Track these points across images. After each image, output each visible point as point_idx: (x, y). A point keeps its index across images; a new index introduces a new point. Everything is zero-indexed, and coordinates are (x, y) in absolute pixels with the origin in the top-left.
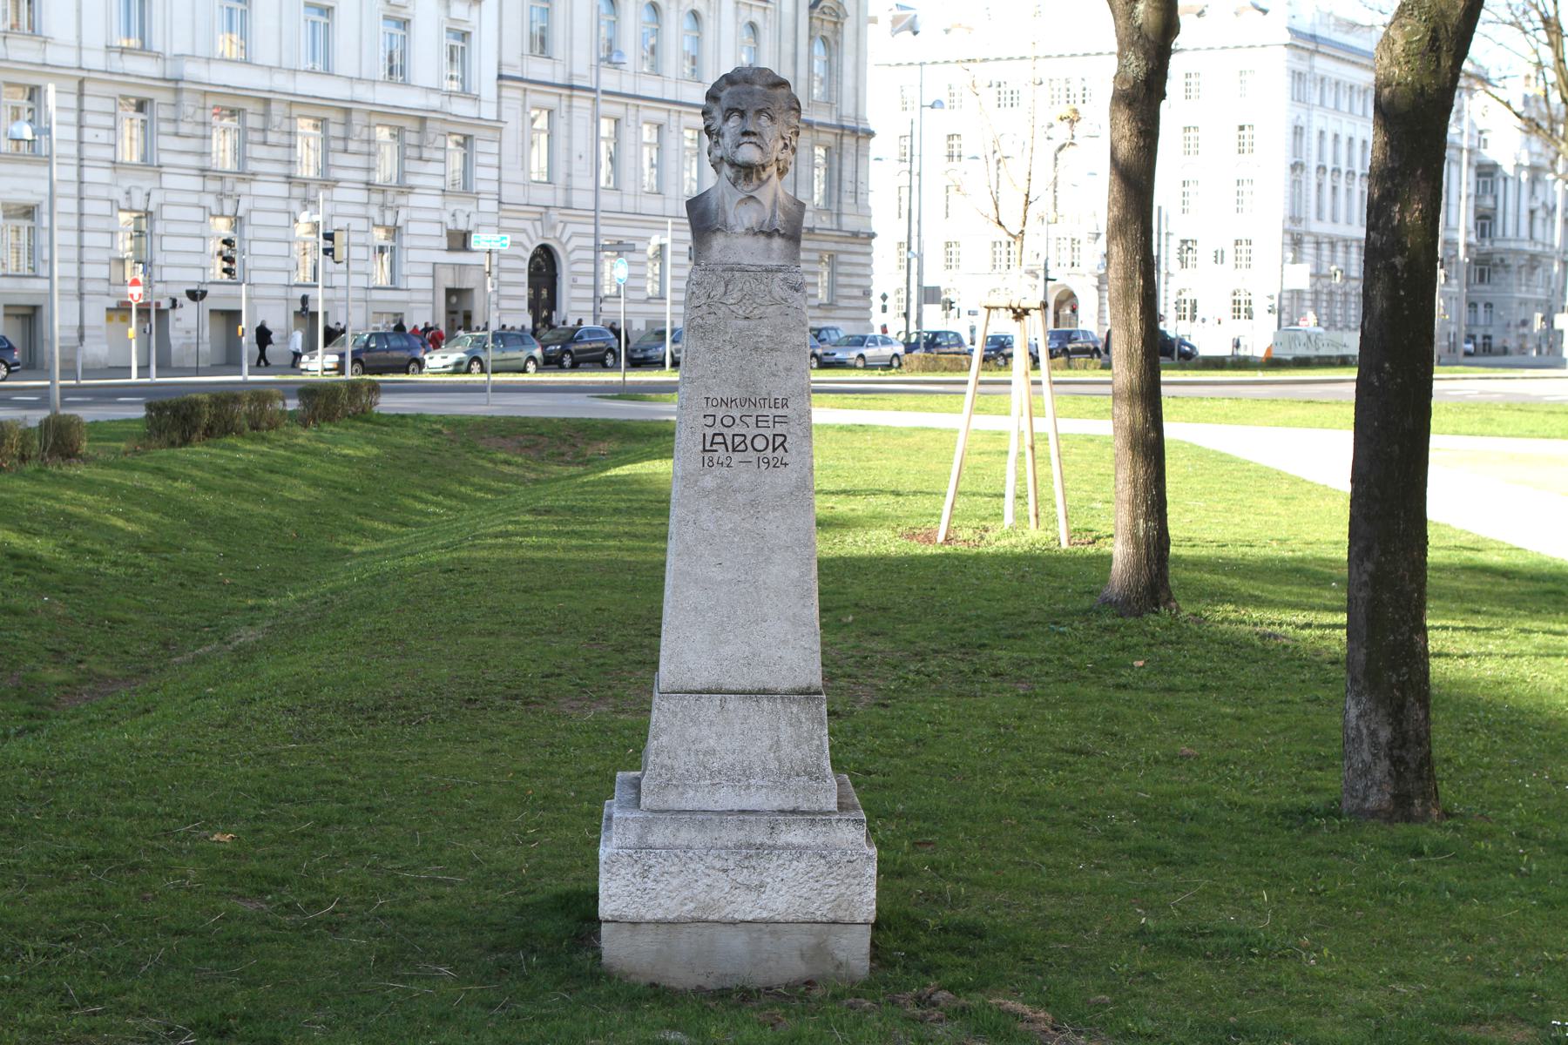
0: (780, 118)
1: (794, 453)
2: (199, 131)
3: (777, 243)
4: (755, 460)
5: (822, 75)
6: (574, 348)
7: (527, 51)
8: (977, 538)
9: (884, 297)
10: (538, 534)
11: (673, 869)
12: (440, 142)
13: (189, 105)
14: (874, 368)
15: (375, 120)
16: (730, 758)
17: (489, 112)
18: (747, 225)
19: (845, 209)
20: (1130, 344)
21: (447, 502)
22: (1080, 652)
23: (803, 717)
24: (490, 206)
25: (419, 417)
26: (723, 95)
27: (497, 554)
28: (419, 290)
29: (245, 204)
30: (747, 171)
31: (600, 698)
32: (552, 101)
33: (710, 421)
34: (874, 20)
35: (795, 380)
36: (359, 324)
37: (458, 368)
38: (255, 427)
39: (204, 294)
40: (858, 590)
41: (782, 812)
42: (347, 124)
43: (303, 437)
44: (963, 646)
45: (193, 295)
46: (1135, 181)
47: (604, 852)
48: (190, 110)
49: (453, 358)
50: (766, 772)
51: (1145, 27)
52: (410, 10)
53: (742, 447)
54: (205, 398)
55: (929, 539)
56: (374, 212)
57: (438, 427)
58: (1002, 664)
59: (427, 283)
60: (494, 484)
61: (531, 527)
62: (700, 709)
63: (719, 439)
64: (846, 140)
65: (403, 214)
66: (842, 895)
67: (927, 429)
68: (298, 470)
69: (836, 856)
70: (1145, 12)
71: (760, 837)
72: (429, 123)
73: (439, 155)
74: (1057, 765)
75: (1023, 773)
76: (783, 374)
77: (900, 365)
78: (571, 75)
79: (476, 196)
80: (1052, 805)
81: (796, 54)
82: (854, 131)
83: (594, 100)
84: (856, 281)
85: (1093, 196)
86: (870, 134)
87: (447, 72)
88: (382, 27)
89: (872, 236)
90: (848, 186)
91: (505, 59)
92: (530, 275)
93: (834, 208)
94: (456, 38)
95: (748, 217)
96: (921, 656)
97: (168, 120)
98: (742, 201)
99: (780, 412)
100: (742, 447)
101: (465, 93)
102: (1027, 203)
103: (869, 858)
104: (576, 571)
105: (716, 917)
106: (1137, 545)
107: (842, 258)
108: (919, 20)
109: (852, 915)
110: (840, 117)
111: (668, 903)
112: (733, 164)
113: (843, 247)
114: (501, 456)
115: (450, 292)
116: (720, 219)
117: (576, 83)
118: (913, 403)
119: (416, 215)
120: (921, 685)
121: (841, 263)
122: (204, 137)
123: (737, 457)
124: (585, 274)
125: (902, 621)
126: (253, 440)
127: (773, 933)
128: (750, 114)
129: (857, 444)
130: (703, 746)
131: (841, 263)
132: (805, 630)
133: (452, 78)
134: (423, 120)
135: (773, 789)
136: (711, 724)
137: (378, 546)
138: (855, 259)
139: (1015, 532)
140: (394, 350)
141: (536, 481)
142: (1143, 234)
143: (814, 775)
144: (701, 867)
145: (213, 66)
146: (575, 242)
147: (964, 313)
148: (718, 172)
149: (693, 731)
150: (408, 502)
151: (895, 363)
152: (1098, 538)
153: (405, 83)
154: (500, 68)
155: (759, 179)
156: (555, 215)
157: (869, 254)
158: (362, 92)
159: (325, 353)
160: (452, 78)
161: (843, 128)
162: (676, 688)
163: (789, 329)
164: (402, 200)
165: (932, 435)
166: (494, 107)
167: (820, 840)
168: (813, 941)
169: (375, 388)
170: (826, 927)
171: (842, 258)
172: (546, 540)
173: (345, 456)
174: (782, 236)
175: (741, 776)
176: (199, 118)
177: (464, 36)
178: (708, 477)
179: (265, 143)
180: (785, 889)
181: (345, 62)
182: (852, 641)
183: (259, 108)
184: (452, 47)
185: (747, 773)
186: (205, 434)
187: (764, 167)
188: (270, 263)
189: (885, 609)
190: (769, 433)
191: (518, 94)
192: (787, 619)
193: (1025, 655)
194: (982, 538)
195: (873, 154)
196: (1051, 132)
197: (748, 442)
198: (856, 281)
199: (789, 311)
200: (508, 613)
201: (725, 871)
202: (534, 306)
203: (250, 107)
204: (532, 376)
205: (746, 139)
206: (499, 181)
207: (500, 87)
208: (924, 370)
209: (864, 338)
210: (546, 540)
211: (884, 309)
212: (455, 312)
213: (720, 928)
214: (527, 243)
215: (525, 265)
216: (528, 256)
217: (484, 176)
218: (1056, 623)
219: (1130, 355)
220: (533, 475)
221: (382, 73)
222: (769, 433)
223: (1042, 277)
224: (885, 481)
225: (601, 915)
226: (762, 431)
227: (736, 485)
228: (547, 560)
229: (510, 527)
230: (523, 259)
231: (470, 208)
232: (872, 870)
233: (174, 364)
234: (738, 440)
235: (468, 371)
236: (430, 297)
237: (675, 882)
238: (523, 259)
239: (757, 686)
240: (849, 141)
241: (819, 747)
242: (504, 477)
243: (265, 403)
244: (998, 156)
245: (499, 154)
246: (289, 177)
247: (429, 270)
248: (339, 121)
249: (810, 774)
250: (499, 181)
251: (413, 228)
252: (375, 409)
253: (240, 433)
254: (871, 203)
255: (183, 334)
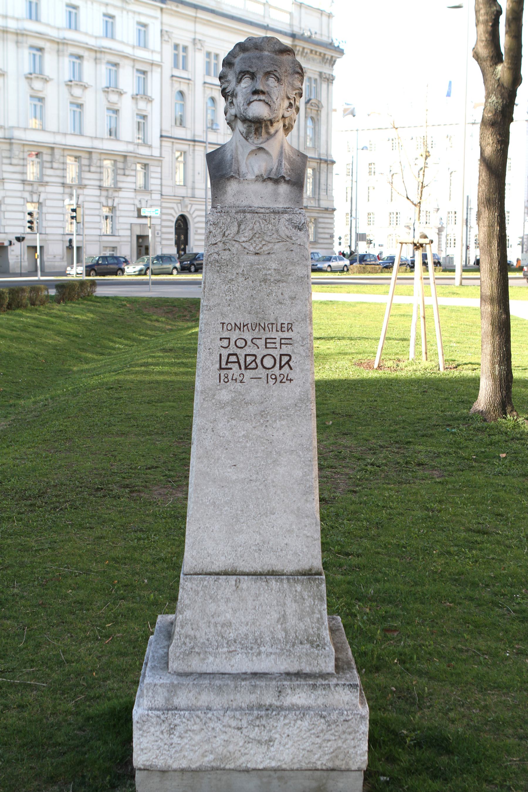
0: (286, 80)
1: (298, 370)
2: (21, 162)
3: (283, 188)
4: (264, 376)
5: (311, 136)
6: (196, 263)
7: (173, 124)
8: (395, 366)
9: (340, 238)
10: (164, 364)
11: (195, 727)
12: (133, 167)
13: (16, 150)
14: (335, 271)
15: (103, 157)
16: (244, 630)
17: (156, 153)
18: (257, 172)
19: (322, 197)
20: (491, 264)
21: (126, 342)
22: (467, 447)
23: (305, 594)
24: (156, 196)
25: (116, 298)
26: (237, 61)
27: (139, 378)
28: (124, 236)
29: (43, 196)
30: (257, 126)
31: (179, 486)
32: (185, 147)
33: (225, 343)
34: (335, 110)
35: (299, 307)
36: (93, 252)
37: (141, 273)
38: (33, 304)
39: (23, 238)
40: (333, 401)
41: (288, 674)
42: (90, 159)
43: (57, 308)
44: (397, 442)
45: (19, 239)
46: (495, 170)
47: (137, 713)
48: (17, 153)
49: (138, 268)
50: (274, 641)
51: (502, 79)
52: (119, 105)
53: (253, 365)
54: (6, 290)
55: (369, 366)
56: (103, 200)
57: (125, 303)
58: (422, 457)
59: (128, 233)
60: (150, 332)
61: (161, 360)
62: (218, 588)
63: (233, 359)
64: (322, 165)
65: (116, 200)
66: (340, 748)
67: (363, 303)
68: (51, 326)
69: (334, 716)
70: (502, 70)
71: (269, 699)
72: (128, 158)
73: (133, 173)
74: (472, 545)
75: (449, 553)
76: (288, 302)
77: (348, 270)
78: (194, 135)
79: (151, 192)
80: (474, 585)
81: (299, 136)
82: (326, 161)
83: (205, 147)
84: (326, 231)
85: (471, 181)
86: (333, 162)
87: (136, 135)
88: (106, 113)
89: (334, 210)
90: (323, 187)
91: (163, 128)
92: (176, 229)
93: (317, 197)
94: (141, 118)
95: (258, 166)
96: (373, 451)
97: (7, 158)
98: (252, 152)
99: (286, 335)
100: (253, 365)
101: (145, 144)
102: (423, 187)
103: (362, 717)
104: (179, 389)
105: (232, 766)
106: (494, 380)
107: (321, 220)
108: (355, 110)
109: (347, 764)
110: (319, 154)
111: (191, 755)
112: (245, 120)
113: (321, 215)
114: (155, 317)
115: (139, 237)
116: (234, 167)
117: (197, 139)
118: (355, 290)
119: (122, 201)
120: (375, 474)
121: (320, 223)
122: (24, 165)
123: (248, 374)
124: (201, 228)
125: (360, 424)
126: (31, 311)
127: (280, 778)
128: (260, 76)
129: (329, 311)
130: (221, 619)
131: (320, 223)
132: (307, 521)
133: (139, 138)
134: (125, 157)
135: (280, 655)
136: (228, 600)
137: (86, 367)
138: (326, 220)
139: (417, 362)
140: (108, 266)
141: (171, 330)
142: (499, 200)
143: (315, 643)
144: (218, 726)
145: (28, 132)
146: (197, 213)
147: (377, 246)
148: (233, 129)
149: (212, 607)
150: (106, 342)
151: (345, 269)
152: (459, 365)
153: (117, 139)
154: (161, 131)
155: (268, 133)
156: (187, 201)
157: (333, 218)
158: (97, 144)
159: (78, 266)
160: (139, 138)
161: (321, 159)
162: (197, 570)
163: (293, 263)
164: (116, 194)
165: (366, 306)
166: (159, 151)
167: (320, 701)
168: (314, 784)
169: (93, 283)
170: (325, 774)
171: (321, 220)
172: (166, 369)
173: (76, 318)
174: (288, 182)
175: (253, 644)
176: (21, 156)
177: (144, 117)
178: (224, 392)
179: (52, 168)
180: (290, 743)
181: (89, 129)
182: (332, 439)
183: (49, 151)
184: (139, 123)
185: (258, 642)
186: (8, 308)
187: (271, 122)
188: (55, 224)
189: (350, 416)
190: (276, 353)
191: (170, 144)
192: (292, 512)
193: (433, 449)
194: (398, 366)
195: (335, 171)
196: (416, 162)
197: (258, 361)
198: (326, 231)
199: (294, 247)
200: (136, 419)
201: (239, 729)
202: (178, 243)
203: (45, 151)
204: (176, 277)
205: (256, 97)
206: (161, 185)
207: (161, 141)
208: (360, 272)
209: (331, 257)
210: (166, 369)
211: (340, 244)
212: (141, 246)
213: (236, 774)
214: (174, 214)
215: (173, 224)
216: (175, 220)
217: (154, 183)
218: (448, 425)
219: (491, 271)
220: (170, 327)
221: (106, 135)
222: (276, 353)
223: (412, 229)
224: (344, 331)
225: (135, 764)
226: (270, 351)
227: (248, 398)
228: (165, 381)
229: (150, 360)
230: (173, 221)
231: (147, 197)
232: (365, 728)
233: (11, 272)
234: (249, 359)
235: (145, 274)
236: (129, 239)
237: (197, 738)
238: (173, 221)
239: (266, 568)
240: (323, 166)
241: (319, 620)
242: (155, 329)
243: (38, 292)
244: (392, 173)
245: (161, 173)
246: (63, 184)
247: (129, 227)
248: (86, 157)
249: (312, 643)
250: (161, 185)
251: (121, 207)
252: (94, 294)
253: (25, 307)
254: (333, 195)
255: (15, 257)
